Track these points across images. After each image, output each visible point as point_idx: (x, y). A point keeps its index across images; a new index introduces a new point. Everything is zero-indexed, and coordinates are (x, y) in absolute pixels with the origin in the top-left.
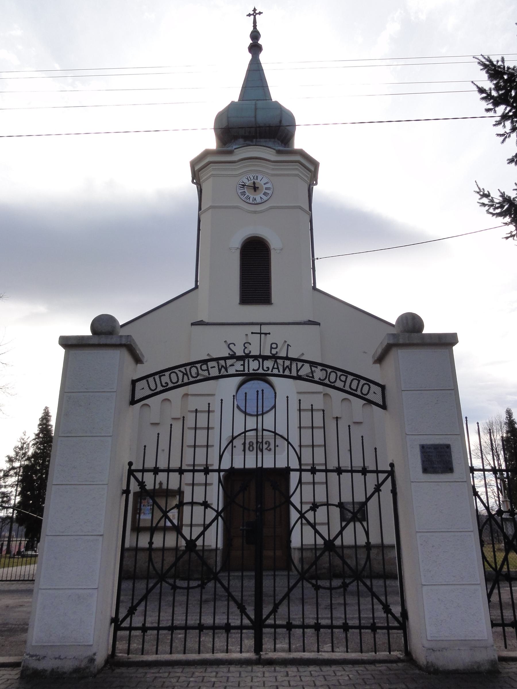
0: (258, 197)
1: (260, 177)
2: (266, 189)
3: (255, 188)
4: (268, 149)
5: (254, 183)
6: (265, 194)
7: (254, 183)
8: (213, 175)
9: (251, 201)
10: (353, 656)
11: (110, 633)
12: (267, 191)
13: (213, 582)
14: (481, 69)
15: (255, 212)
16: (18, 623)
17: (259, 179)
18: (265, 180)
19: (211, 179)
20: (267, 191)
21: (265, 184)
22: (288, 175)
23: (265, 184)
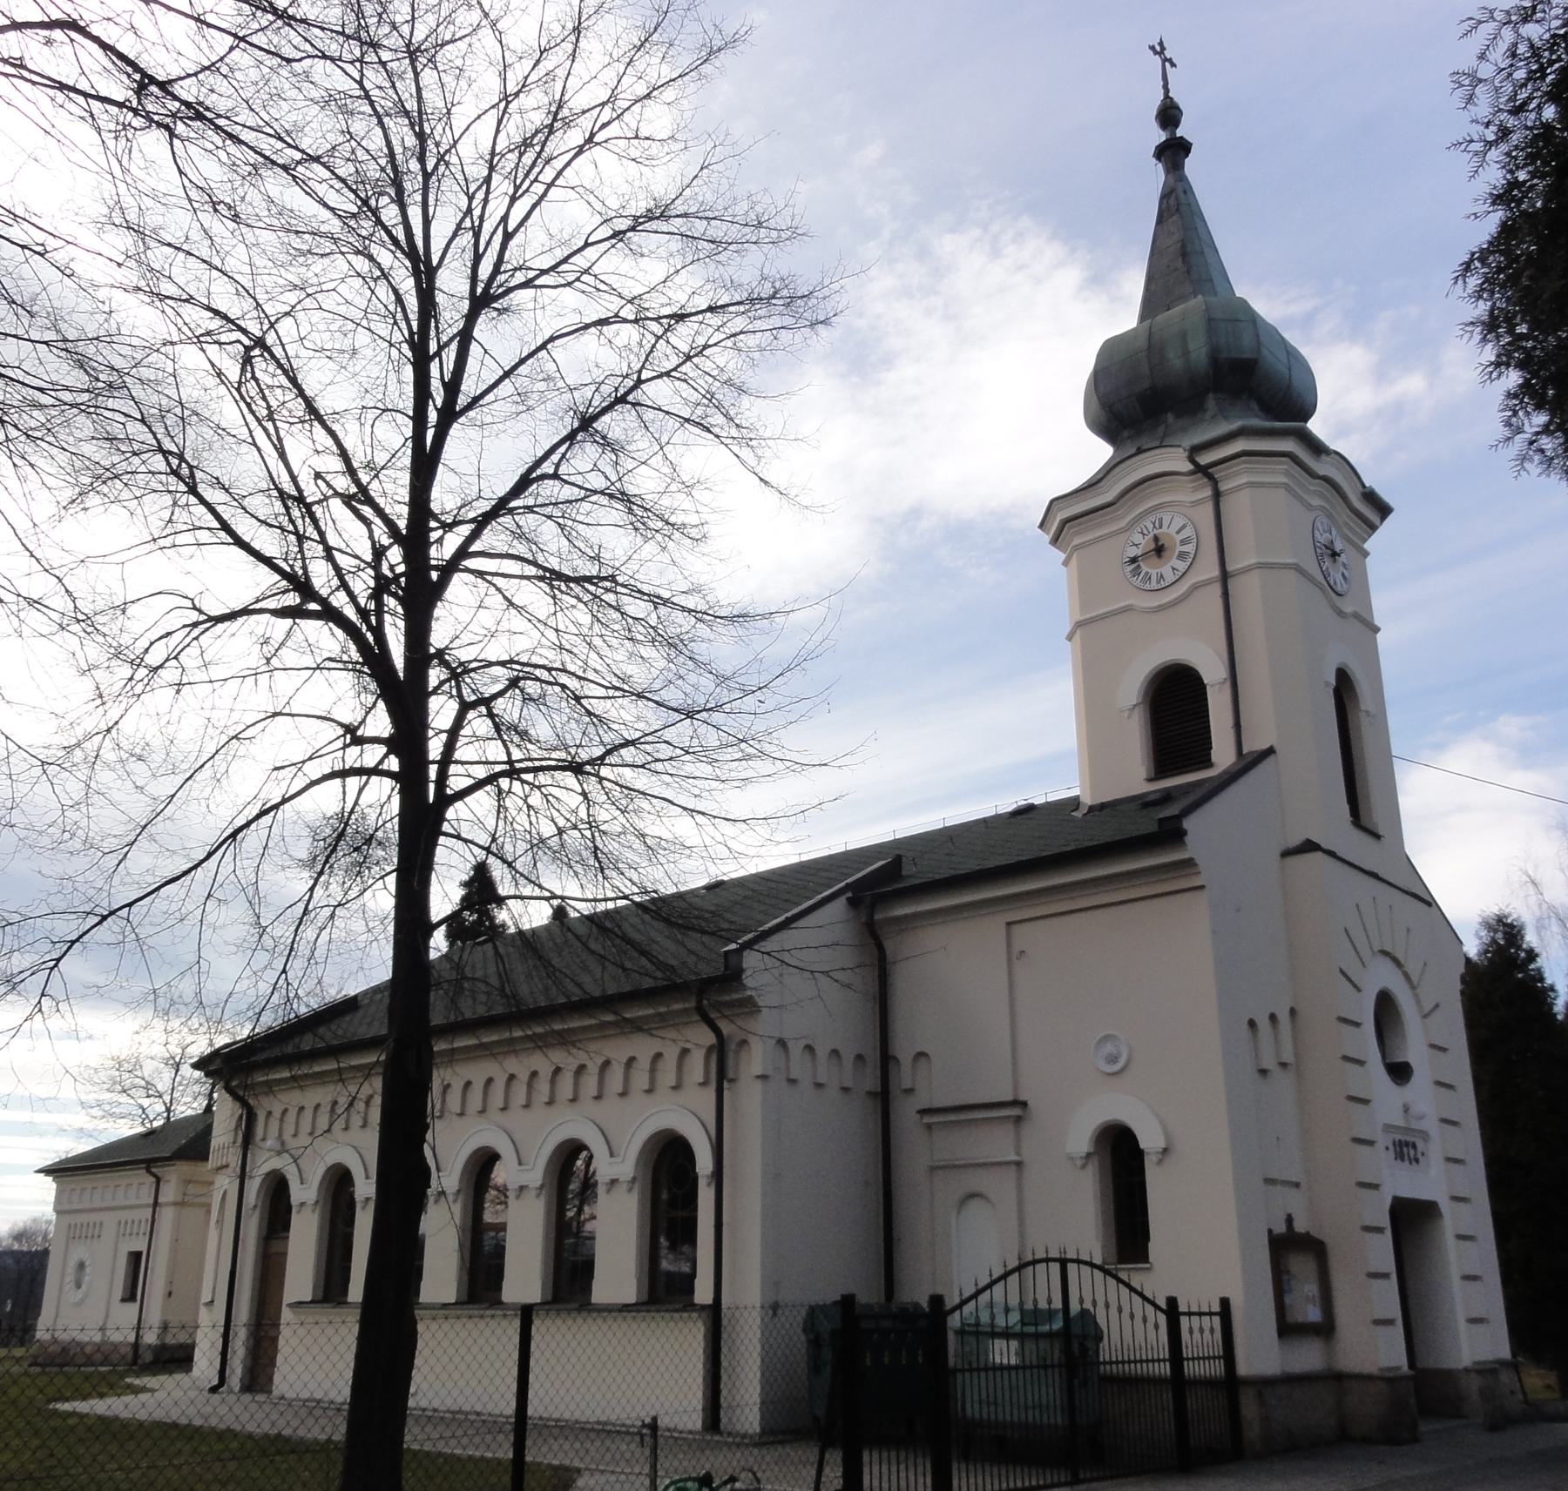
6: (1182, 556)
8: (1252, 485)
17: (1165, 524)
19: (1246, 492)
21: (1178, 532)
23: (1178, 532)
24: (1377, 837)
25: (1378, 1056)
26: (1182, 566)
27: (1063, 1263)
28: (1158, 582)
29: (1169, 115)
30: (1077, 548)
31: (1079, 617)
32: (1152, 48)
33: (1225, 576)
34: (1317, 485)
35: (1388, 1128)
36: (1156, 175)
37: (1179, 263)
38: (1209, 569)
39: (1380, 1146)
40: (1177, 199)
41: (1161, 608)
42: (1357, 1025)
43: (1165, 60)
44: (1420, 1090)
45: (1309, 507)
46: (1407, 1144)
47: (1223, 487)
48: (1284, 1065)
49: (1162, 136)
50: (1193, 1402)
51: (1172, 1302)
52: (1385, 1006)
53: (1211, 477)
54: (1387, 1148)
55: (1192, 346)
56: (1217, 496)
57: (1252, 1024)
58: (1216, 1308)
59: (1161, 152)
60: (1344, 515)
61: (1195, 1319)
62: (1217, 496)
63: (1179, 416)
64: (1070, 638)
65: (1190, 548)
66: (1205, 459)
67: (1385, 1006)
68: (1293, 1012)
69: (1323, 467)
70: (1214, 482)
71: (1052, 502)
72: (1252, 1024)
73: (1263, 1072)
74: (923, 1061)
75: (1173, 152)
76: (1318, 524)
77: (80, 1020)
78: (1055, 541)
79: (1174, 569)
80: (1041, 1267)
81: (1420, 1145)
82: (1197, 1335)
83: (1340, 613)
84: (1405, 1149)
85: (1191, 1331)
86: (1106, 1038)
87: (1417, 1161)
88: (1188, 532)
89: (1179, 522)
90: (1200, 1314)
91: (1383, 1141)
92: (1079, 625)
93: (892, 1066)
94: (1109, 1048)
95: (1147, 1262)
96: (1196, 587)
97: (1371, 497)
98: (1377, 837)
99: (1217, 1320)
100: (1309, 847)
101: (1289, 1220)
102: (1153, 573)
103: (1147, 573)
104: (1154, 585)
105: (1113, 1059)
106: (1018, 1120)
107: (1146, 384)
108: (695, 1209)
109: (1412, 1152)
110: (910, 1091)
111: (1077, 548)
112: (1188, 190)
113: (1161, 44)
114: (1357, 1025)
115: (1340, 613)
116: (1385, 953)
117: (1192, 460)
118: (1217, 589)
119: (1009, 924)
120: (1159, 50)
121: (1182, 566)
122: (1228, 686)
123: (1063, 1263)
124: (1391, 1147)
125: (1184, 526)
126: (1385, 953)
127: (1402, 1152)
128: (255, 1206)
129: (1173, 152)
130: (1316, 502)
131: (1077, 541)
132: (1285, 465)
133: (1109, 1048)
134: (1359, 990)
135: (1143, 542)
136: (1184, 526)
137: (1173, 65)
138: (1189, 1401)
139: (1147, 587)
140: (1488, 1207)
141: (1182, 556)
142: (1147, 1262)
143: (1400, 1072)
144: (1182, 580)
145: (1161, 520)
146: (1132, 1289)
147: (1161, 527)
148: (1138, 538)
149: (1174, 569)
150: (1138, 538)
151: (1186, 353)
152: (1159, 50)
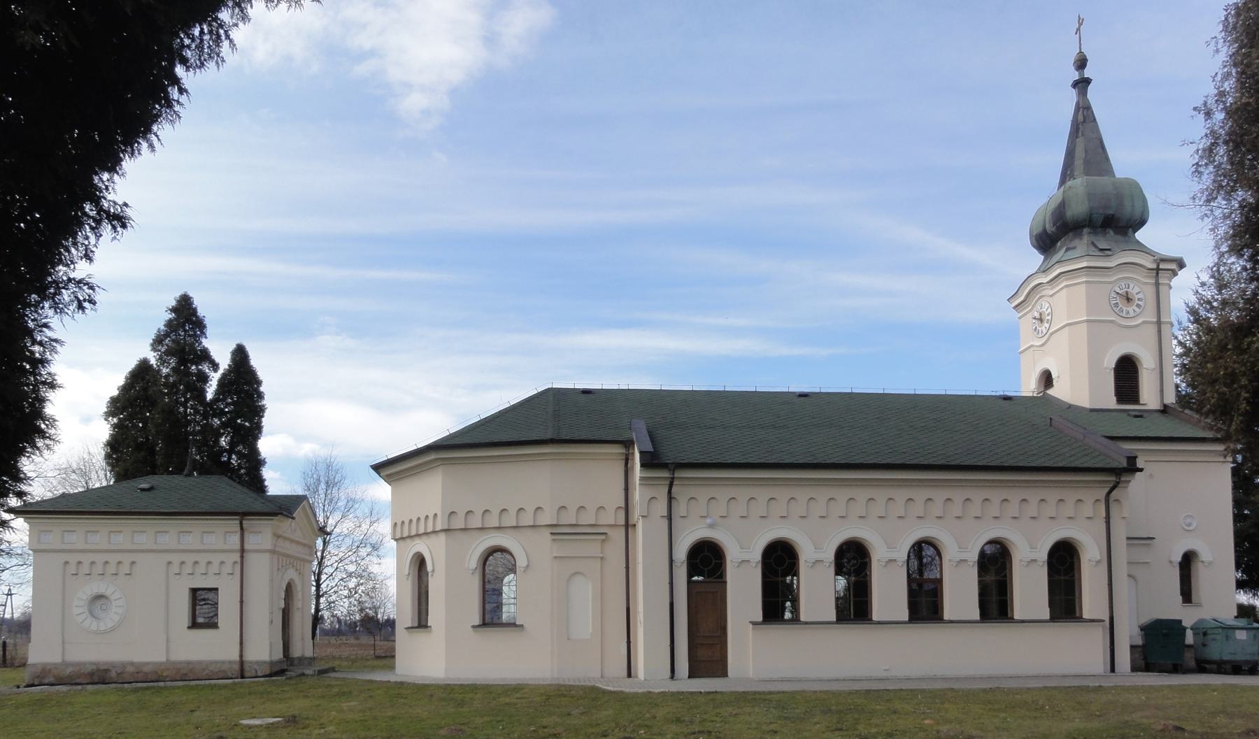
0: (1132, 309)
1: (1131, 286)
2: (1139, 299)
3: (1129, 300)
4: (1143, 253)
5: (1127, 293)
6: (1138, 306)
7: (1127, 293)
8: (1067, 286)
9: (1124, 315)
10: (675, 727)
11: (431, 565)
12: (1139, 302)
13: (513, 575)
14: (151, 146)
15: (1127, 327)
16: (64, 466)
17: (1131, 288)
18: (1137, 289)
19: (1064, 290)
20: (1139, 302)
21: (1137, 294)
22: (1102, 282)
23: (1137, 294)
29: (1081, 63)
36: (1072, 96)
49: (1076, 76)
59: (1075, 84)
63: (1116, 233)
75: (1082, 84)
77: (1063, 337)
94: (1188, 520)
102: (1125, 309)
103: (1121, 308)
105: (1189, 525)
106: (603, 541)
107: (1111, 212)
108: (980, 582)
128: (409, 574)
129: (1082, 84)
133: (1188, 520)
141: (1138, 306)
144: (1120, 317)
151: (1133, 206)
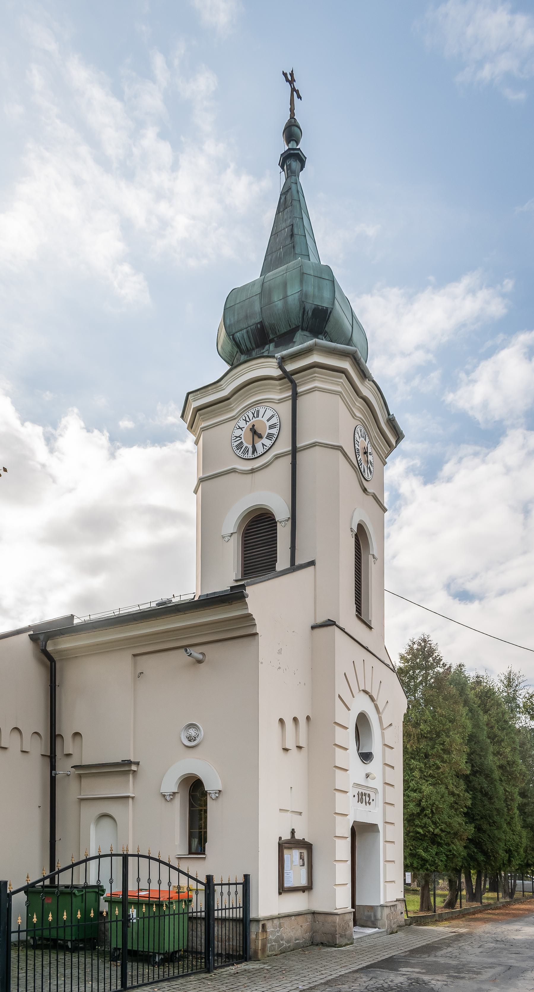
6: (269, 436)
17: (261, 414)
21: (268, 420)
23: (268, 420)
24: (371, 628)
25: (355, 748)
26: (268, 443)
27: (125, 857)
28: (253, 453)
30: (204, 429)
31: (201, 475)
32: (285, 74)
33: (294, 451)
34: (359, 403)
35: (357, 785)
37: (288, 241)
38: (284, 446)
39: (350, 794)
40: (292, 196)
41: (253, 471)
42: (346, 728)
43: (293, 90)
44: (375, 766)
45: (354, 416)
46: (365, 794)
47: (300, 390)
48: (299, 747)
50: (217, 930)
51: (209, 878)
52: (362, 719)
53: (292, 381)
54: (354, 796)
55: (290, 299)
56: (295, 397)
57: (281, 721)
58: (241, 880)
60: (374, 432)
61: (225, 888)
62: (295, 397)
64: (196, 492)
65: (274, 431)
66: (290, 367)
67: (362, 719)
68: (308, 718)
69: (366, 390)
70: (294, 386)
71: (189, 394)
72: (281, 721)
73: (286, 750)
74: (78, 739)
76: (358, 429)
78: (191, 426)
79: (263, 445)
80: (105, 861)
81: (373, 796)
82: (225, 896)
83: (365, 490)
84: (364, 797)
85: (222, 894)
86: (192, 726)
87: (370, 803)
88: (274, 420)
89: (269, 413)
90: (229, 884)
91: (353, 791)
92: (201, 480)
93: (58, 742)
94: (192, 732)
95: (204, 854)
96: (277, 457)
97: (392, 422)
98: (371, 628)
99: (240, 888)
100: (330, 623)
101: (293, 832)
104: (250, 455)
105: (190, 739)
107: (258, 319)
109: (367, 799)
110: (69, 755)
111: (204, 429)
112: (299, 191)
113: (292, 74)
114: (346, 728)
115: (365, 490)
116: (365, 692)
117: (281, 367)
118: (289, 459)
119: (135, 655)
120: (290, 79)
121: (268, 443)
122: (289, 523)
123: (125, 857)
124: (356, 796)
125: (272, 416)
126: (365, 692)
127: (362, 798)
130: (358, 414)
131: (203, 425)
132: (343, 379)
133: (192, 732)
134: (349, 709)
135: (246, 426)
136: (272, 416)
137: (299, 97)
138: (216, 929)
139: (246, 456)
140: (286, 733)
142: (204, 854)
143: (366, 757)
145: (258, 412)
146: (180, 871)
147: (258, 416)
148: (242, 424)
149: (263, 445)
150: (242, 424)
152: (290, 79)
